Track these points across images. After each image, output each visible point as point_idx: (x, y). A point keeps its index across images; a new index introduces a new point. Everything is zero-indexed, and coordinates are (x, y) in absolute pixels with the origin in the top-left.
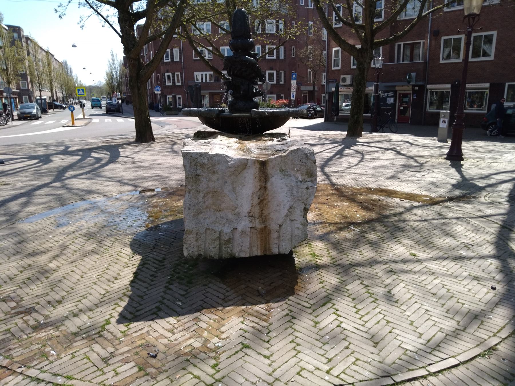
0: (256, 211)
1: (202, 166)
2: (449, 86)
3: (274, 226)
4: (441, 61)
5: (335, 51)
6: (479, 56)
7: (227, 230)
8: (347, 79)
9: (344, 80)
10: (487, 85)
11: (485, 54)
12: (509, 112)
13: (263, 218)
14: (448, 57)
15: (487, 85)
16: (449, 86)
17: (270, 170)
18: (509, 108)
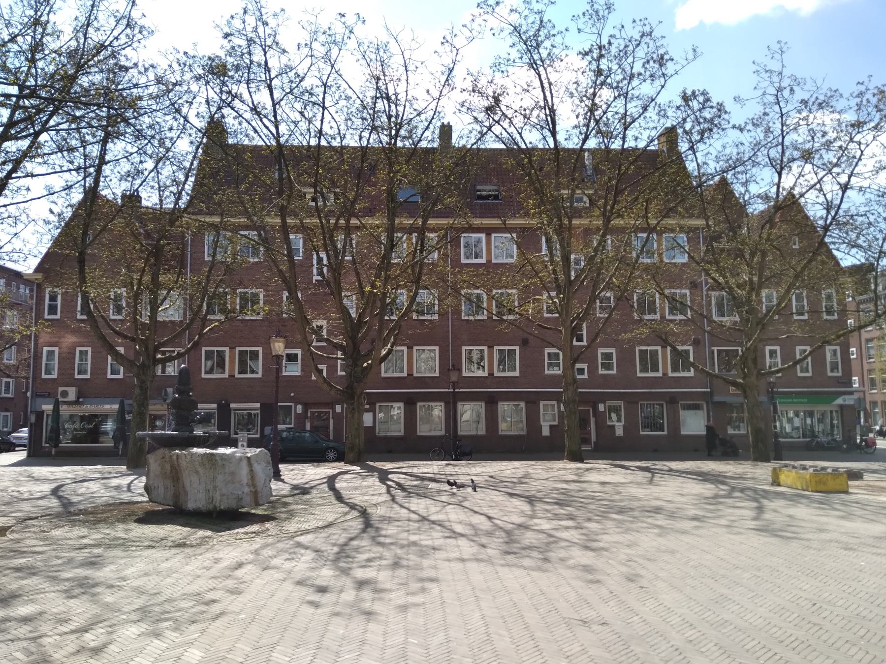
0: (250, 482)
1: (225, 460)
2: (215, 406)
3: (259, 489)
4: (203, 376)
5: (49, 352)
6: (246, 372)
8: (70, 393)
9: (64, 394)
10: (258, 405)
11: (253, 372)
12: (284, 434)
13: (254, 485)
14: (210, 371)
15: (258, 405)
16: (215, 406)
17: (252, 462)
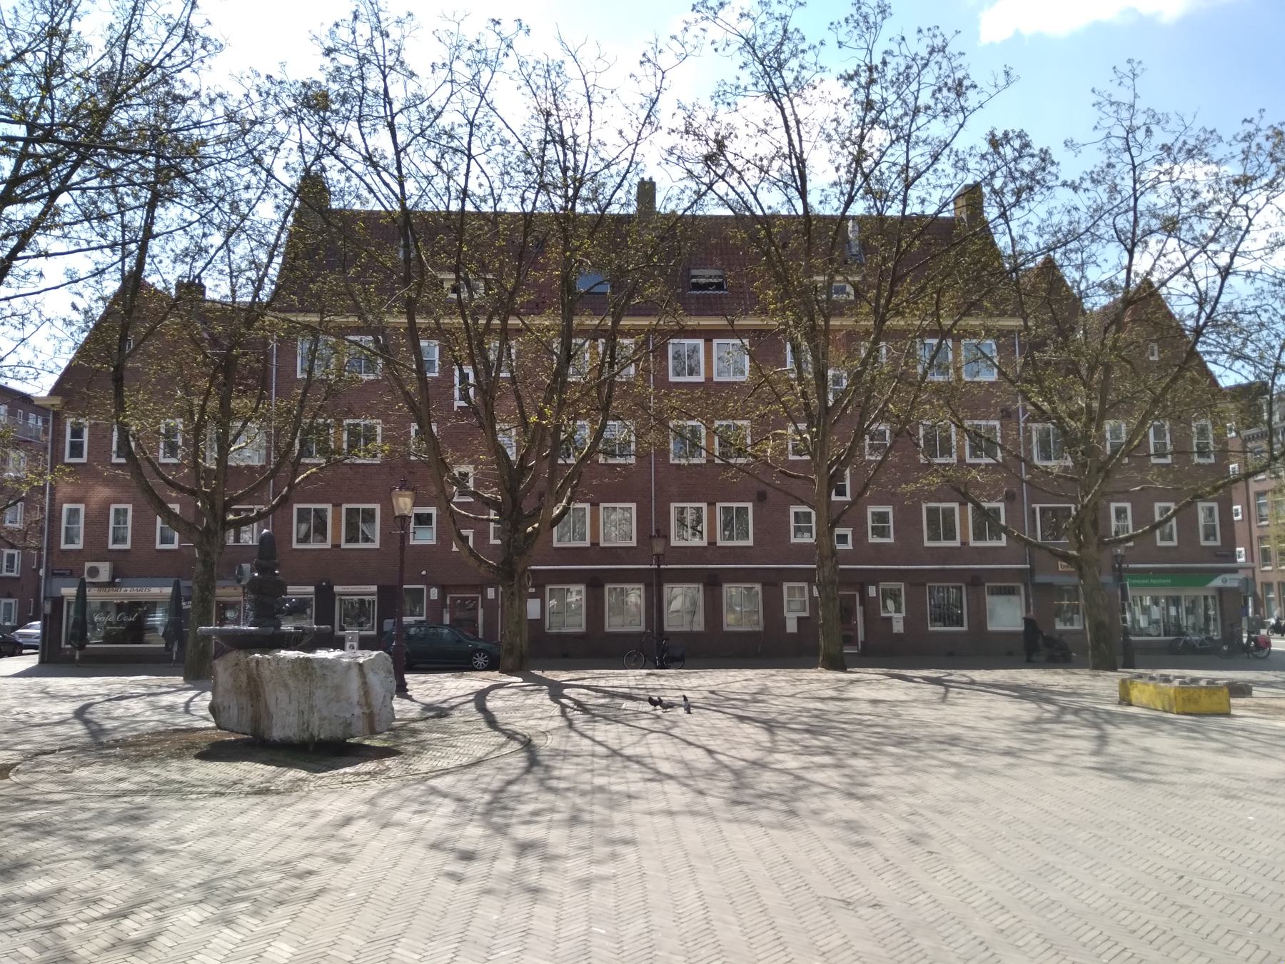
0: (363, 700)
2: (311, 589)
3: (376, 711)
4: (295, 545)
5: (70, 510)
6: (357, 541)
7: (348, 716)
8: (101, 571)
9: (93, 572)
10: (374, 588)
11: (367, 539)
12: (413, 631)
13: (368, 705)
14: (305, 539)
15: (374, 588)
16: (311, 589)
17: (366, 670)
18: (410, 625)
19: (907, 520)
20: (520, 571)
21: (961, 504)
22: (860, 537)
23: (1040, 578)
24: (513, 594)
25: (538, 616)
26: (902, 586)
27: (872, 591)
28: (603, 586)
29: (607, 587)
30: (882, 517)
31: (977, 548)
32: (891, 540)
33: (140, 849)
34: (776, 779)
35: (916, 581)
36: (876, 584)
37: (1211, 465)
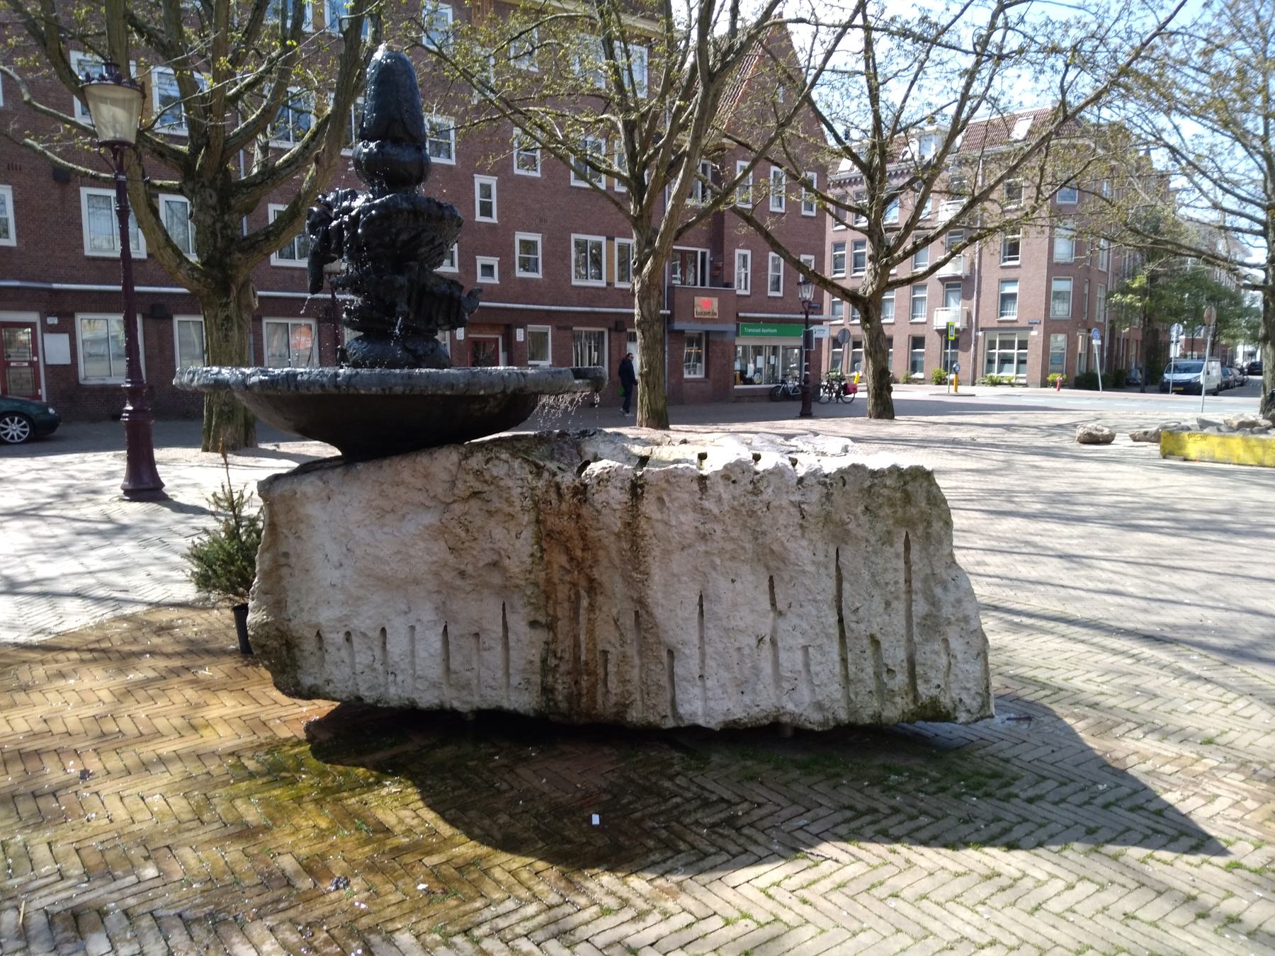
19: (557, 255)
20: (241, 279)
21: (608, 238)
22: (507, 269)
23: (678, 326)
24: (228, 318)
25: (66, 360)
26: (548, 329)
27: (520, 335)
28: (171, 319)
29: (176, 319)
30: (528, 246)
31: (621, 290)
32: (538, 275)
33: (574, 929)
34: (1004, 561)
35: (562, 322)
36: (523, 326)
37: (576, 232)
